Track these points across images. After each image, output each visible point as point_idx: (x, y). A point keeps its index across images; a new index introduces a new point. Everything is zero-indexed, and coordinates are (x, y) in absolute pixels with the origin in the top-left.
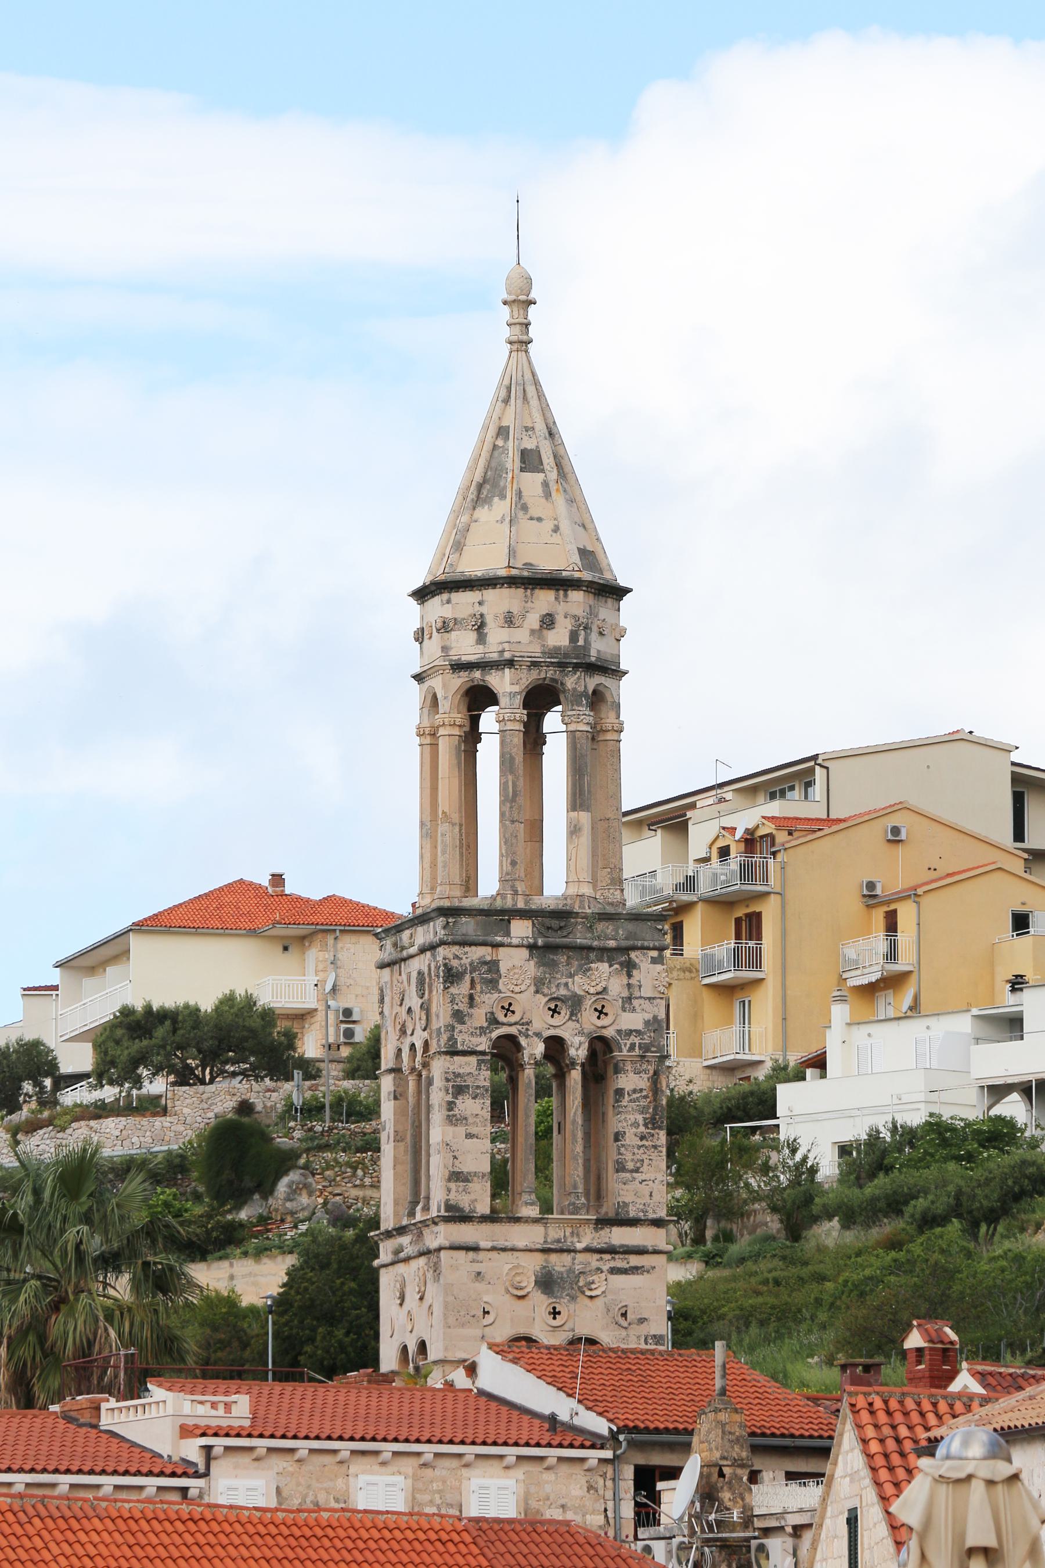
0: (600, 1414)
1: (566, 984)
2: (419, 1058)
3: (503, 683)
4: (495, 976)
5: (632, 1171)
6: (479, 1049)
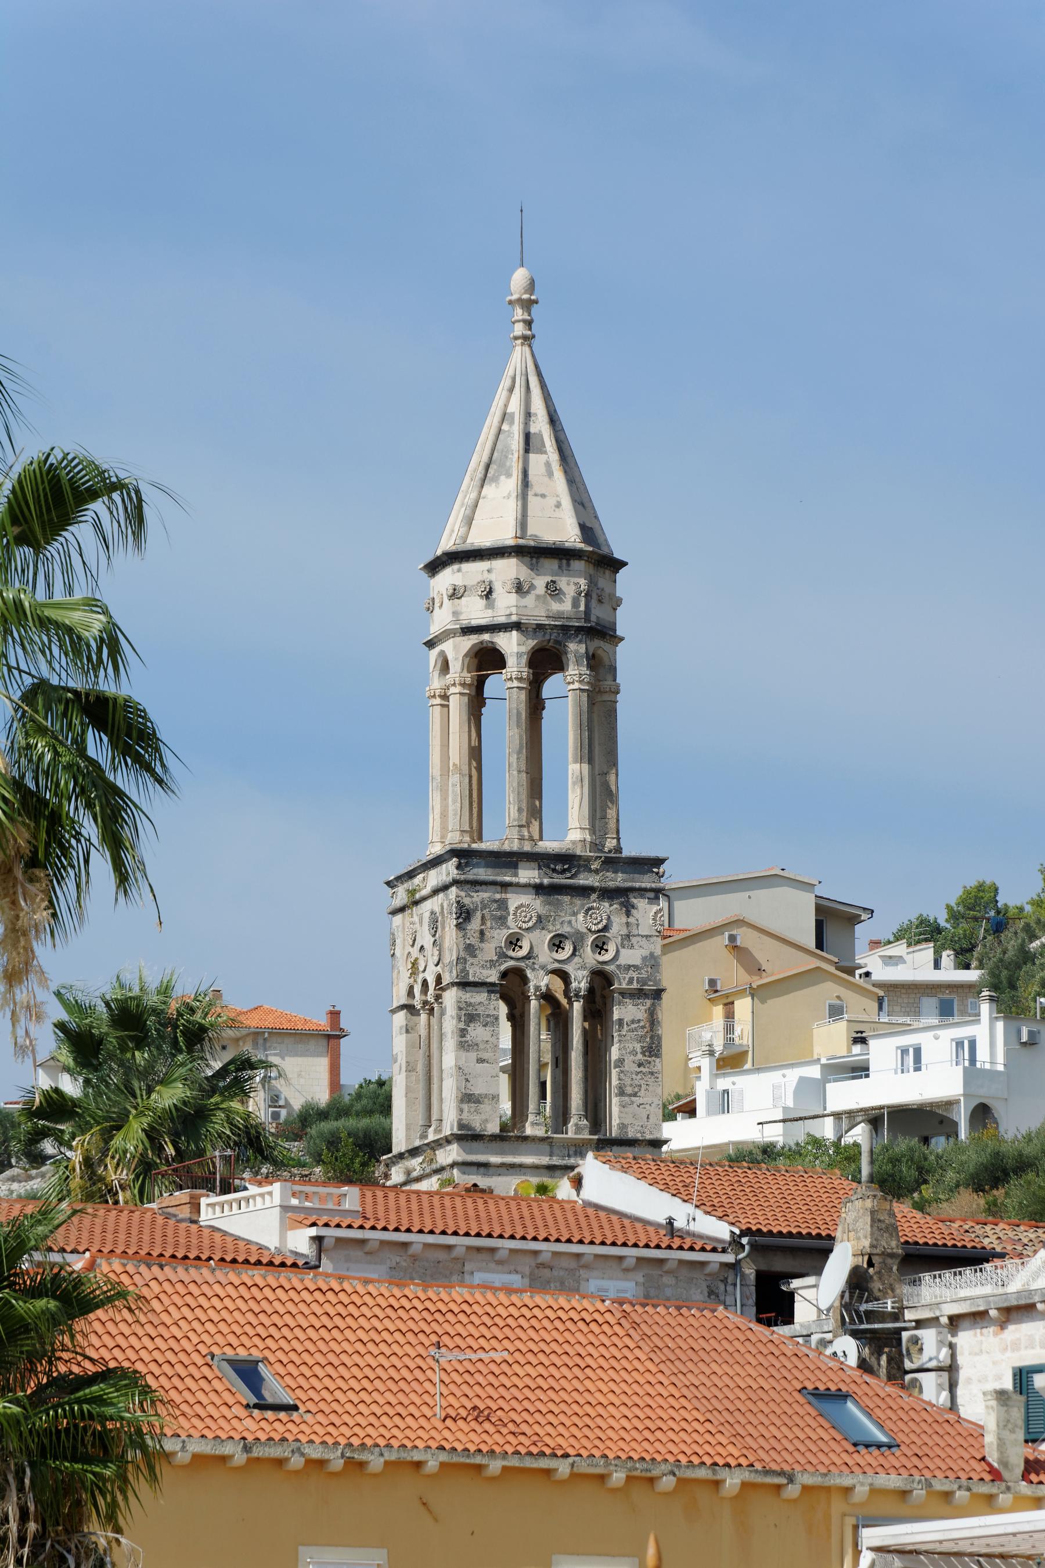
0: (720, 1218)
1: (570, 922)
2: (431, 991)
3: (510, 645)
4: (504, 913)
5: (630, 1095)
6: (489, 980)
